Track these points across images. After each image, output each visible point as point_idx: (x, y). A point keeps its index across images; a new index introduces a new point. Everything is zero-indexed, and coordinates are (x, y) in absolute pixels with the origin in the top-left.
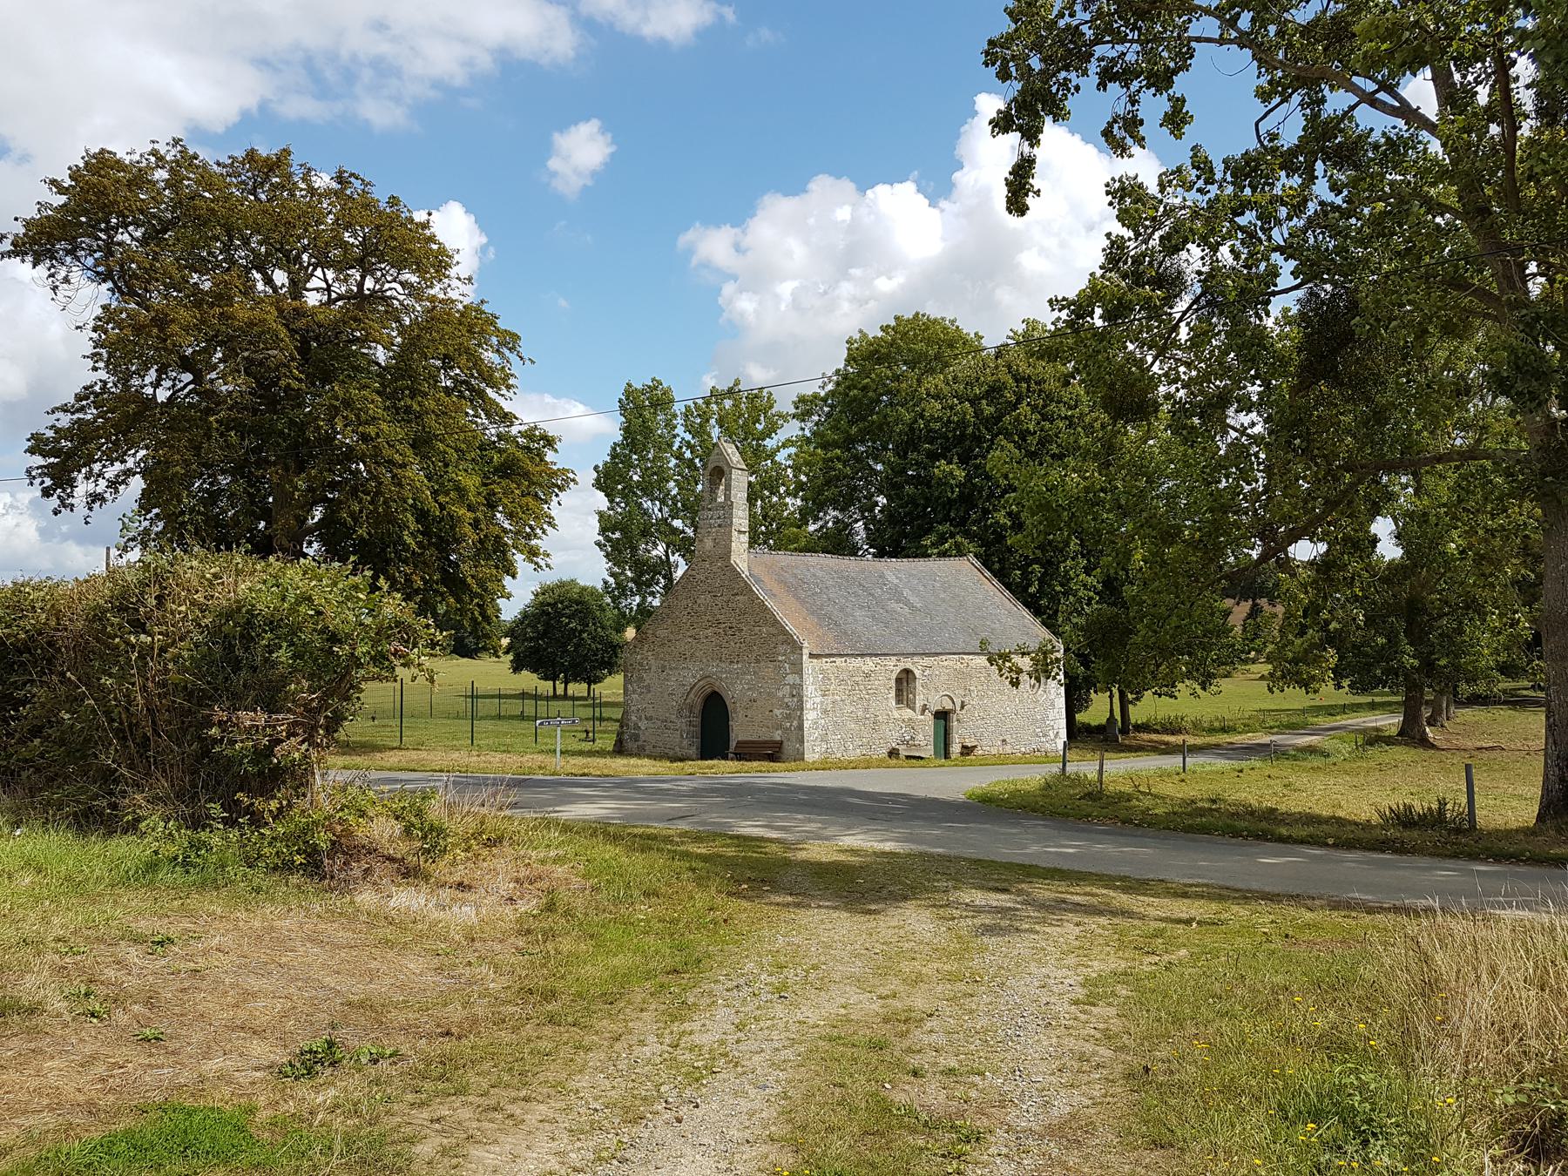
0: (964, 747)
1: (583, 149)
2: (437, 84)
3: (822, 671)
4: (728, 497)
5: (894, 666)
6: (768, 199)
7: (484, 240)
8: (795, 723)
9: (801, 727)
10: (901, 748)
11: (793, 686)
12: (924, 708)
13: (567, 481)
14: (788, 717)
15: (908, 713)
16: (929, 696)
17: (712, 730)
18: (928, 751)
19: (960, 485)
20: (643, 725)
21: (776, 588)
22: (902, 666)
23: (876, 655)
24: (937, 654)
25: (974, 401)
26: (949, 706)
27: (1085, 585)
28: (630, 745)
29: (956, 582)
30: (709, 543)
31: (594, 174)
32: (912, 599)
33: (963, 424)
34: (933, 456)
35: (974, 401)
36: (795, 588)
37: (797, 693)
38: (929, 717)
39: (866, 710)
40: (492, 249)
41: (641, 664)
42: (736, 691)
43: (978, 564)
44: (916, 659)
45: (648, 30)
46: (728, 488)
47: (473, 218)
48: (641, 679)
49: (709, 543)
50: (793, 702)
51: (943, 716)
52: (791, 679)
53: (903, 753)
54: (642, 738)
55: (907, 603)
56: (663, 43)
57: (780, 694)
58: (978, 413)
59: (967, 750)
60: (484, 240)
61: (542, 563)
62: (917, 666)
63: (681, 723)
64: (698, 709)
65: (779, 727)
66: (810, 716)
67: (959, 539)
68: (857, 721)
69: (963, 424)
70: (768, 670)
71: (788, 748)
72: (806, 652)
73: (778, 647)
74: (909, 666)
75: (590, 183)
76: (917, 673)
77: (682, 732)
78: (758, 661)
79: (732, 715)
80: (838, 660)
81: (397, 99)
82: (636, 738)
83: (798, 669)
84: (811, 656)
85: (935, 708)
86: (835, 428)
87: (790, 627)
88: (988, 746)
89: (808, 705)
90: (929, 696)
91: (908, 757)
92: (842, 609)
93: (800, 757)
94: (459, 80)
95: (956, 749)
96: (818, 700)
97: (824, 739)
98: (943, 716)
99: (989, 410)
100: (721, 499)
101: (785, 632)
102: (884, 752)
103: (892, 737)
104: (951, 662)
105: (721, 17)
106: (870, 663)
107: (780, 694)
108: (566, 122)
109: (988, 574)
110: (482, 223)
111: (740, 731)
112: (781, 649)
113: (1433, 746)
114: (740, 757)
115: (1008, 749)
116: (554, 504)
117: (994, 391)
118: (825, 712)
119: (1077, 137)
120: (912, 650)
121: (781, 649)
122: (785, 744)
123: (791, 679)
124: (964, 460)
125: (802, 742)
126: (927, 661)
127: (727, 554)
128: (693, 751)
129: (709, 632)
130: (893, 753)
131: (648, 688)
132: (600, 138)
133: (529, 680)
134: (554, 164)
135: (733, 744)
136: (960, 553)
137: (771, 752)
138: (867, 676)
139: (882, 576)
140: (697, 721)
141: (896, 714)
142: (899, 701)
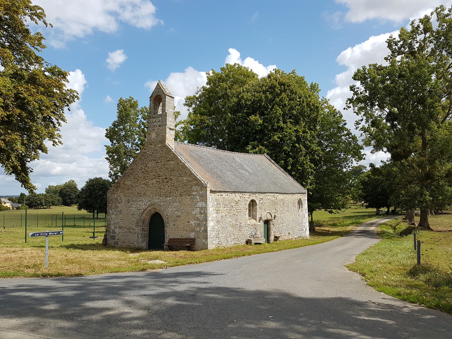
0: (275, 237)
1: (118, 57)
2: (75, 36)
3: (216, 200)
4: (164, 110)
5: (248, 198)
6: (171, 74)
7: (86, 82)
8: (202, 228)
9: (206, 231)
10: (252, 239)
11: (202, 208)
12: (261, 218)
13: (73, 97)
14: (199, 225)
15: (253, 221)
16: (262, 213)
17: (156, 235)
18: (263, 240)
19: (260, 125)
20: (117, 231)
21: (189, 159)
22: (251, 198)
23: (241, 192)
24: (265, 193)
25: (264, 92)
26: (269, 218)
27: (310, 167)
28: (110, 242)
29: (257, 165)
30: (153, 135)
31: (120, 64)
32: (248, 169)
33: (261, 100)
34: (249, 114)
35: (264, 92)
36: (198, 159)
37: (204, 212)
38: (262, 223)
39: (236, 220)
40: (88, 85)
41: (116, 199)
42: (169, 211)
43: (269, 157)
44: (257, 195)
45: (138, 26)
46: (164, 106)
47: (84, 75)
48: (117, 207)
49: (153, 135)
50: (201, 217)
51: (267, 222)
52: (200, 204)
53: (253, 242)
54: (117, 238)
55: (246, 170)
56: (142, 30)
57: (194, 213)
58: (266, 97)
59: (276, 238)
60: (86, 82)
61: (57, 140)
62: (257, 198)
63: (138, 230)
64: (147, 222)
65: (193, 230)
66: (211, 224)
67: (260, 147)
68: (233, 226)
69: (261, 100)
70: (187, 200)
71: (198, 242)
72: (208, 190)
73: (193, 187)
74: (254, 198)
75: (119, 66)
76: (257, 202)
77: (138, 236)
78: (181, 195)
79: (166, 225)
80: (224, 194)
81: (62, 40)
82: (113, 238)
83: (204, 198)
84: (212, 192)
85: (264, 218)
86: (205, 108)
87: (199, 177)
88: (284, 237)
89: (209, 218)
90: (262, 213)
91: (256, 244)
92: (221, 171)
93: (205, 247)
94: (81, 35)
95: (272, 238)
96: (214, 215)
97: (217, 237)
98: (267, 222)
99: (270, 96)
100: (160, 112)
101: (196, 179)
102: (244, 241)
103: (247, 234)
104: (270, 197)
105: (160, 23)
106: (237, 197)
107: (194, 213)
108: (114, 49)
109: (273, 162)
110: (86, 77)
111: (171, 233)
112: (194, 188)
113: (432, 230)
114: (171, 248)
115: (291, 237)
116: (66, 109)
117: (272, 87)
118: (218, 222)
119: (257, 62)
120: (255, 191)
121: (194, 188)
122: (197, 241)
123: (200, 204)
124: (262, 114)
125: (206, 238)
126: (262, 196)
127: (164, 140)
128: (144, 245)
129: (154, 181)
130: (248, 242)
131: (120, 212)
132: (122, 55)
133: (84, 212)
134: (108, 60)
135: (167, 240)
136: (260, 152)
137: (188, 245)
138: (237, 203)
139: (234, 159)
140: (147, 228)
141: (249, 222)
142: (250, 216)
